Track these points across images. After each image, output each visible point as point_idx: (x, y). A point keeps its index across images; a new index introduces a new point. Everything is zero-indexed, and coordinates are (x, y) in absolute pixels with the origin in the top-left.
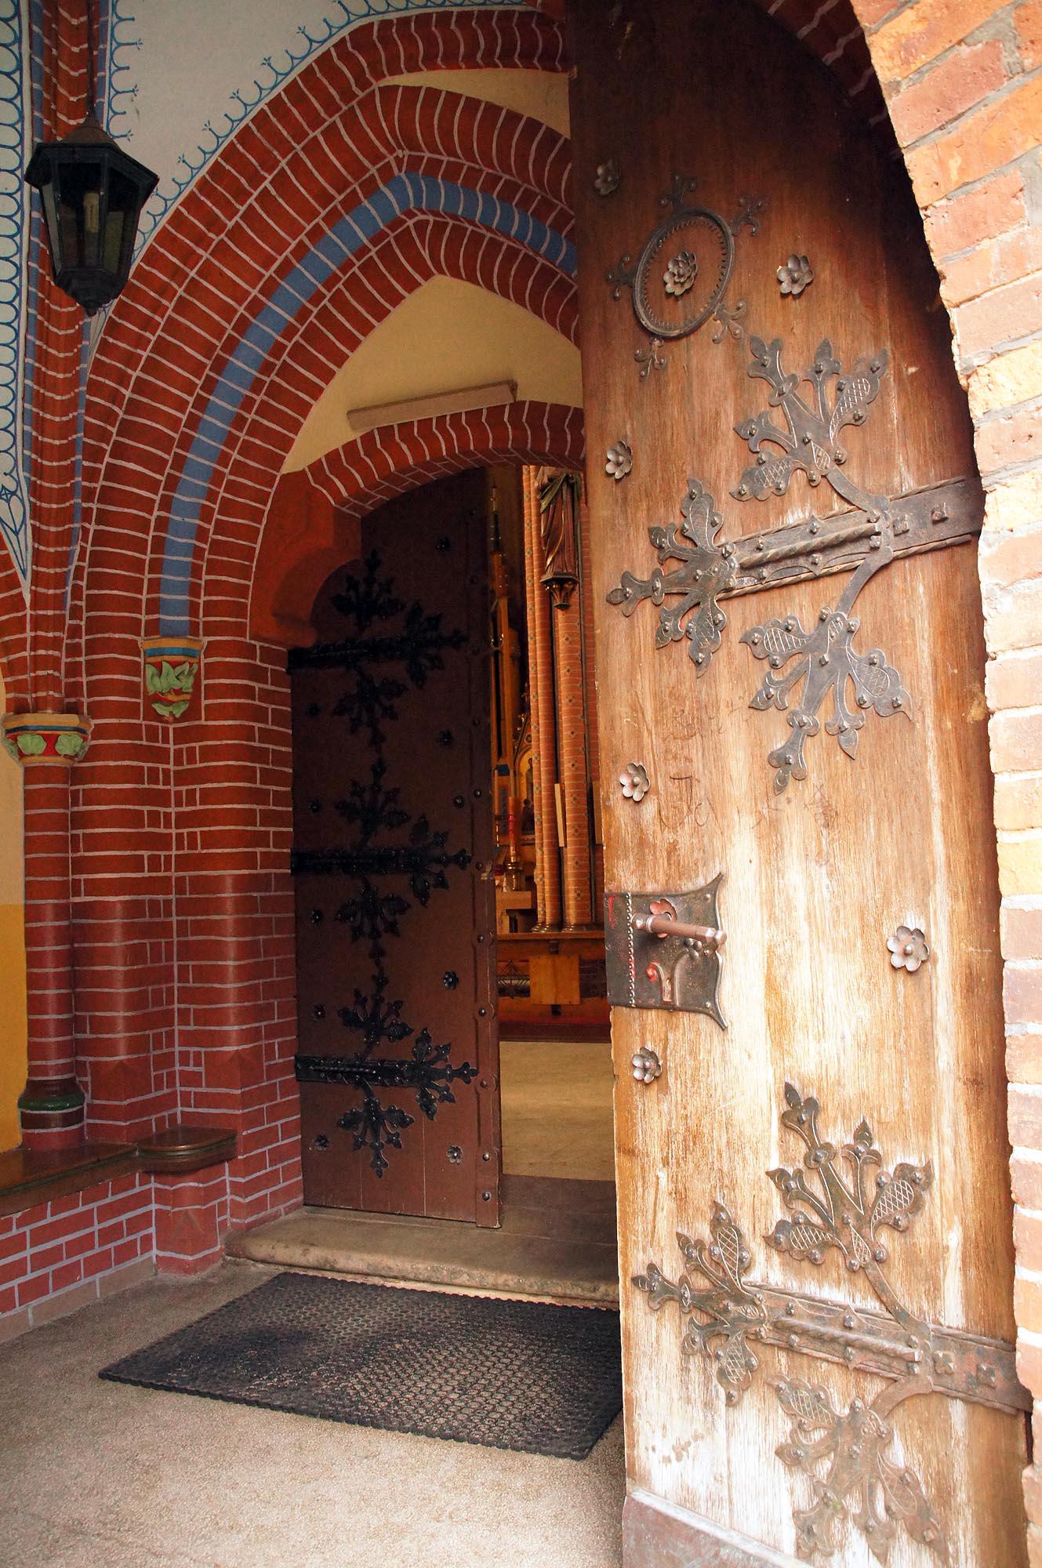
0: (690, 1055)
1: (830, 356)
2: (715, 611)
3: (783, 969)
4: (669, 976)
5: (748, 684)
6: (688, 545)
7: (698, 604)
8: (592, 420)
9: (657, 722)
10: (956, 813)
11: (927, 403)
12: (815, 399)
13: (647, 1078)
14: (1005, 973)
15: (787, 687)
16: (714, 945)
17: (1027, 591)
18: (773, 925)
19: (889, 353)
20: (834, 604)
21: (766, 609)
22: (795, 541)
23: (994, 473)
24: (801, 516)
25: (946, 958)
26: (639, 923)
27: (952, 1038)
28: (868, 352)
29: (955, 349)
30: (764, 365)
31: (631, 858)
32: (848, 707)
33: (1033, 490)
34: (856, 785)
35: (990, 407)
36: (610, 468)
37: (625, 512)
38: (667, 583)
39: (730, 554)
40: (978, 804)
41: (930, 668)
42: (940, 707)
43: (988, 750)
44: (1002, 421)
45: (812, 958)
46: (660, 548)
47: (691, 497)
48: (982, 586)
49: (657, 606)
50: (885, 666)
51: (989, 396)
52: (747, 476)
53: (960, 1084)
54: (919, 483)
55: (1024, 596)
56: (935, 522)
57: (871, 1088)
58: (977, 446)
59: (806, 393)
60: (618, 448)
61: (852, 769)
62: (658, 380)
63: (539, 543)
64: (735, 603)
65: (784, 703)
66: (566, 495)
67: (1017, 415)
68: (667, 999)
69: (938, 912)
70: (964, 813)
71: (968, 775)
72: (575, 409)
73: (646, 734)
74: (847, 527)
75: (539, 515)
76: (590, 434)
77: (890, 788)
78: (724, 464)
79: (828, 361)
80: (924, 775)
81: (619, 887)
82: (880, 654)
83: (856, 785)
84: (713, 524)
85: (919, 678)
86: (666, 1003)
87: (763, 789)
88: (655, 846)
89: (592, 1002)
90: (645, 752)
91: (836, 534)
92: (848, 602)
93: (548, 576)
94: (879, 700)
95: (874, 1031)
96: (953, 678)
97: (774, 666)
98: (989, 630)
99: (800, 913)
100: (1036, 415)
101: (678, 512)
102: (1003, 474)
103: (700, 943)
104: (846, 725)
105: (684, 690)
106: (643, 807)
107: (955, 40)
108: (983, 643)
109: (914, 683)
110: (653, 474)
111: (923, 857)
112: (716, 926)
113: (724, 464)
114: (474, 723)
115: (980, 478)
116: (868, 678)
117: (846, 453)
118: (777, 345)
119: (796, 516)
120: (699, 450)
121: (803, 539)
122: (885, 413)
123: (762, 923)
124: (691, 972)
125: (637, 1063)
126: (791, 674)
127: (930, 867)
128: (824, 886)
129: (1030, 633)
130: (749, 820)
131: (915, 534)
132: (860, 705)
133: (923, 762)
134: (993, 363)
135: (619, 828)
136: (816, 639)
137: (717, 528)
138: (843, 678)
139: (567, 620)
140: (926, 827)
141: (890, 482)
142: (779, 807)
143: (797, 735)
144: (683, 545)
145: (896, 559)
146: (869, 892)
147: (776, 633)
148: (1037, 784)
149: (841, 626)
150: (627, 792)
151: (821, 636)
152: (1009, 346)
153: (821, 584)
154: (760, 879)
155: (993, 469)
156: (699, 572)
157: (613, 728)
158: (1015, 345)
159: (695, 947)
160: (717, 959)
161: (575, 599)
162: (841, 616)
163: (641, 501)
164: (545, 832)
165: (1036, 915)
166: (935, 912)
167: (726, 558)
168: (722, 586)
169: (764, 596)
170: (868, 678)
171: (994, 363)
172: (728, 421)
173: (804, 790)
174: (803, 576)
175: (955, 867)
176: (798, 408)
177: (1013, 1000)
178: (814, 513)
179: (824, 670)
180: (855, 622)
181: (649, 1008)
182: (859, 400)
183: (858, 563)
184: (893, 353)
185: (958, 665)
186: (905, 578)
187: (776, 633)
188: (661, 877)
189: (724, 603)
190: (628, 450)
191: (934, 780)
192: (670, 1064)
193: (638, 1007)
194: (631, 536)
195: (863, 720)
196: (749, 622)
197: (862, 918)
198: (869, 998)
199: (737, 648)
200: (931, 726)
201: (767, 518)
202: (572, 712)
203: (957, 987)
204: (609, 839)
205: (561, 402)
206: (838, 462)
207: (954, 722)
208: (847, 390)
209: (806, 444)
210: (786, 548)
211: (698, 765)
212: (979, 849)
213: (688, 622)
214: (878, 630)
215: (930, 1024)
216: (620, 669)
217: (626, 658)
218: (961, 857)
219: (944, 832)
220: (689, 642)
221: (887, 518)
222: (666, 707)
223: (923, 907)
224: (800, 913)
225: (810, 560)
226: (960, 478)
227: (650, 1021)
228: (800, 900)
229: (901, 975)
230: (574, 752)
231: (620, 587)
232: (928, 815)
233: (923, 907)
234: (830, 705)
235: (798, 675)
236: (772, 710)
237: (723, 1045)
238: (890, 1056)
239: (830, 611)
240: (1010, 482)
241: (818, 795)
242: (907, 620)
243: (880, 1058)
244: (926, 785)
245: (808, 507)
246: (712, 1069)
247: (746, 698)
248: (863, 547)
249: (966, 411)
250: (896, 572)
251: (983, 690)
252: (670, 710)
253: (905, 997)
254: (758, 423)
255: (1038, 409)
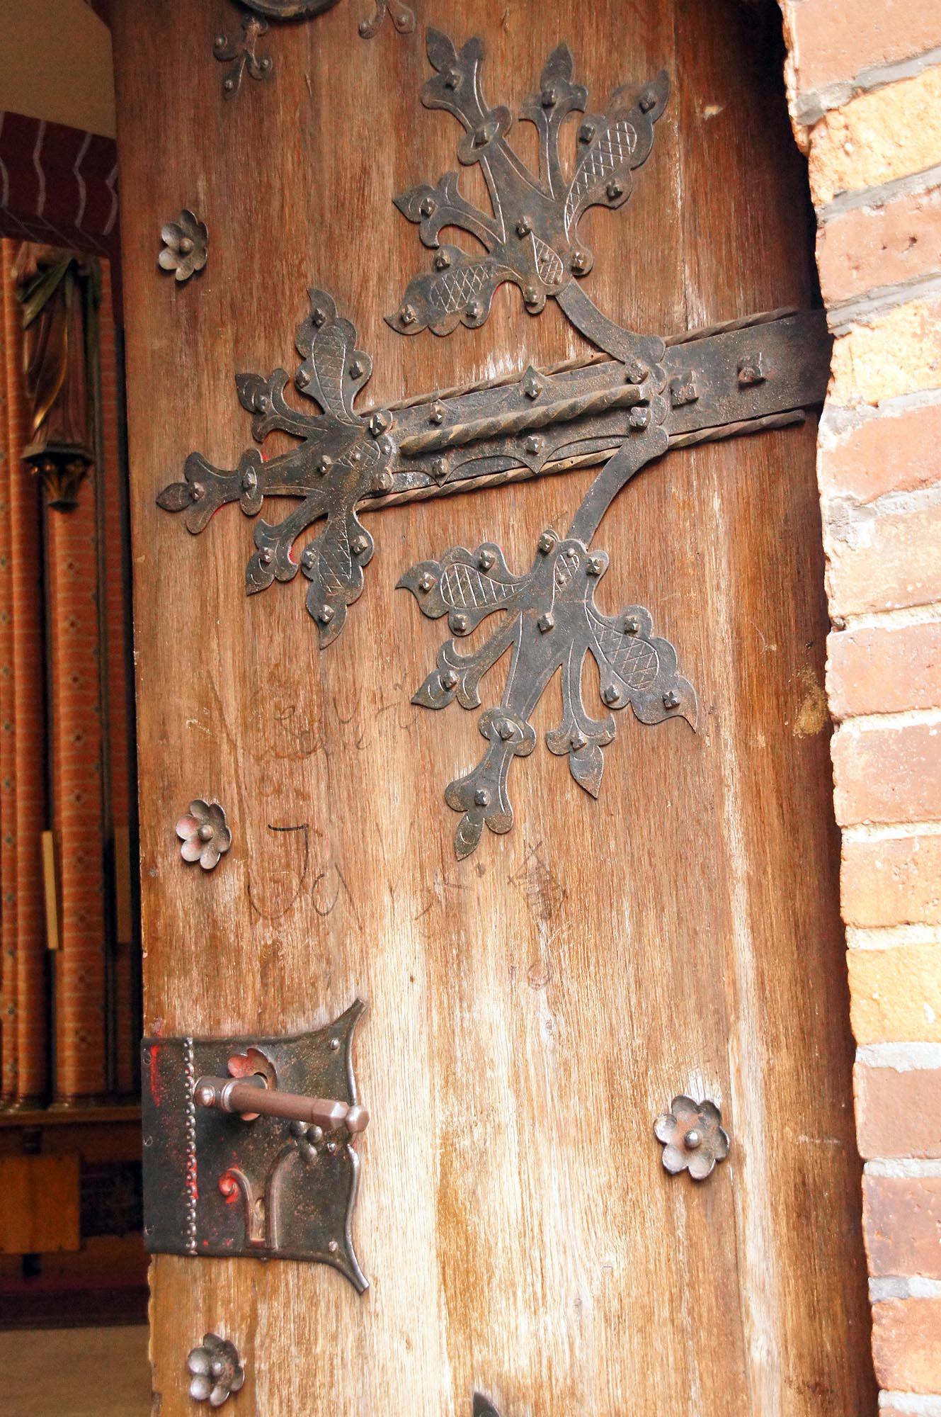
0: (298, 1343)
1: (568, 77)
2: (354, 531)
3: (470, 1177)
4: (260, 1193)
5: (411, 663)
6: (308, 410)
7: (323, 517)
8: (132, 167)
9: (246, 727)
10: (774, 895)
11: (736, 173)
12: (540, 157)
13: (216, 1396)
14: (866, 1182)
15: (479, 669)
16: (345, 1134)
17: (901, 511)
18: (452, 1098)
19: (673, 78)
20: (565, 526)
21: (445, 530)
22: (498, 410)
23: (848, 303)
24: (511, 366)
25: (760, 1154)
26: (208, 1095)
27: (774, 1303)
28: (636, 74)
29: (790, 77)
30: (449, 86)
31: (195, 973)
32: (587, 706)
33: (915, 335)
34: (599, 844)
35: (846, 186)
36: (165, 259)
37: (192, 344)
38: (269, 477)
39: (383, 429)
40: (813, 880)
41: (729, 641)
42: (746, 709)
43: (831, 786)
44: (866, 210)
45: (521, 1156)
46: (257, 412)
47: (315, 322)
48: (824, 501)
49: (250, 517)
50: (652, 636)
51: (844, 164)
52: (418, 289)
53: (791, 1393)
54: (718, 318)
55: (897, 520)
56: (743, 387)
57: (631, 1402)
58: (822, 254)
59: (524, 143)
60: (182, 224)
61: (593, 816)
62: (257, 99)
63: (20, 386)
64: (390, 518)
65: (473, 698)
66: (71, 296)
67: (892, 201)
68: (256, 1237)
69: (745, 1071)
70: (789, 895)
71: (794, 829)
72: (96, 138)
73: (225, 748)
74: (589, 390)
75: (19, 331)
76: (131, 198)
77: (659, 850)
78: (375, 266)
79: (565, 86)
80: (717, 827)
81: (170, 1027)
82: (644, 615)
83: (599, 844)
84: (354, 374)
85: (710, 657)
86: (256, 1246)
87: (437, 852)
88: (238, 950)
89: (106, 1246)
90: (224, 779)
91: (571, 401)
92: (588, 524)
93: (35, 448)
94: (641, 695)
95: (634, 1292)
96: (769, 658)
97: (457, 631)
98: (833, 579)
99: (501, 1073)
100: (924, 201)
101: (290, 351)
102: (865, 305)
103: (319, 1131)
104: (583, 737)
105: (297, 670)
106: (219, 881)
108: (822, 600)
109: (702, 666)
110: (244, 277)
111: (717, 974)
112: (348, 1099)
113: (375, 266)
115: (825, 312)
116: (621, 657)
117: (591, 257)
118: (475, 50)
119: (501, 364)
120: (331, 238)
121: (512, 407)
122: (661, 188)
123: (432, 1091)
124: (305, 1184)
125: (198, 1366)
126: (487, 647)
127: (729, 991)
129: (903, 584)
130: (409, 905)
131: (708, 406)
132: (608, 703)
133: (715, 805)
134: (856, 104)
135: (174, 917)
136: (531, 586)
137: (359, 382)
138: (578, 654)
139: (72, 531)
140: (722, 921)
141: (665, 311)
142: (464, 882)
143: (497, 753)
144: (299, 410)
145: (673, 449)
146: (623, 1035)
147: (461, 573)
148: (917, 848)
149: (577, 564)
150: (188, 852)
151: (539, 580)
152: (883, 75)
153: (544, 488)
154: (429, 1010)
155: (847, 296)
156: (327, 460)
157: (164, 735)
158: (895, 73)
159: (310, 1137)
160: (350, 1160)
161: (86, 492)
162: (577, 547)
163: (223, 324)
164: (21, 923)
165: (919, 1078)
166: (738, 1071)
167: (375, 437)
168: (368, 486)
169: (442, 507)
170: (621, 657)
171: (857, 104)
172: (384, 187)
173: (507, 855)
174: (511, 474)
175: (773, 991)
176: (509, 173)
177: (882, 1233)
178: (533, 363)
179: (545, 640)
180: (600, 557)
181: (224, 1256)
182: (617, 162)
183: (608, 454)
184: (680, 80)
185: (778, 637)
186: (689, 484)
187: (461, 573)
188: (250, 1009)
189: (370, 516)
190: (201, 229)
191: (735, 837)
192: (262, 1366)
194: (204, 390)
195: (611, 729)
196: (414, 552)
197: (610, 1082)
198: (624, 1229)
199: (392, 598)
200: (730, 742)
201: (450, 366)
202: (78, 700)
203: (781, 1208)
204: (154, 939)
205: (66, 122)
206: (578, 273)
207: (772, 736)
208: (596, 142)
209: (521, 237)
210: (482, 423)
211: (318, 808)
212: (814, 961)
213: (302, 549)
214: (640, 574)
215: (733, 1276)
216: (180, 631)
217: (191, 609)
218: (783, 973)
219: (753, 929)
220: (307, 585)
221: (659, 376)
222: (263, 699)
223: (719, 1064)
224: (501, 1073)
225: (524, 445)
226: (790, 309)
227: (223, 1282)
228: (500, 1048)
229: (680, 1186)
230: (79, 775)
231: (182, 480)
232: (725, 898)
233: (719, 1064)
234: (555, 703)
235: (498, 648)
236: (454, 709)
237: (360, 1324)
238: (663, 1339)
239: (559, 537)
240: (875, 319)
241: (533, 861)
242: (690, 556)
243: (647, 1342)
244: (721, 845)
245: (523, 351)
246: (338, 1373)
247: (407, 687)
248: (618, 425)
249: (805, 190)
250: (675, 474)
251: (822, 683)
252: (270, 706)
253: (688, 1226)
254: (437, 195)
255: (929, 191)
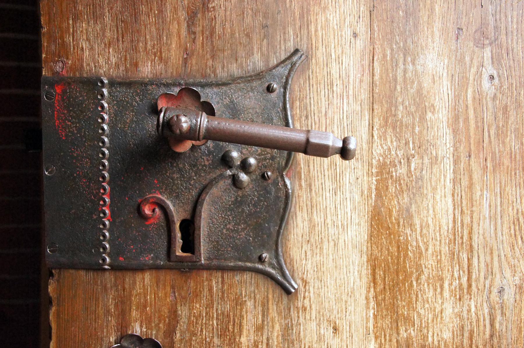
193: (114, 268)
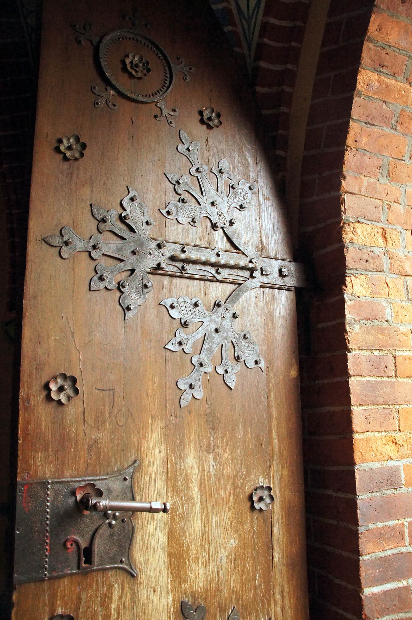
53: (284, 568)
107: (383, 99)
114: (371, 292)
128: (211, 466)
130: (159, 423)
166: (273, 476)
197: (234, 483)
224: (195, 485)
